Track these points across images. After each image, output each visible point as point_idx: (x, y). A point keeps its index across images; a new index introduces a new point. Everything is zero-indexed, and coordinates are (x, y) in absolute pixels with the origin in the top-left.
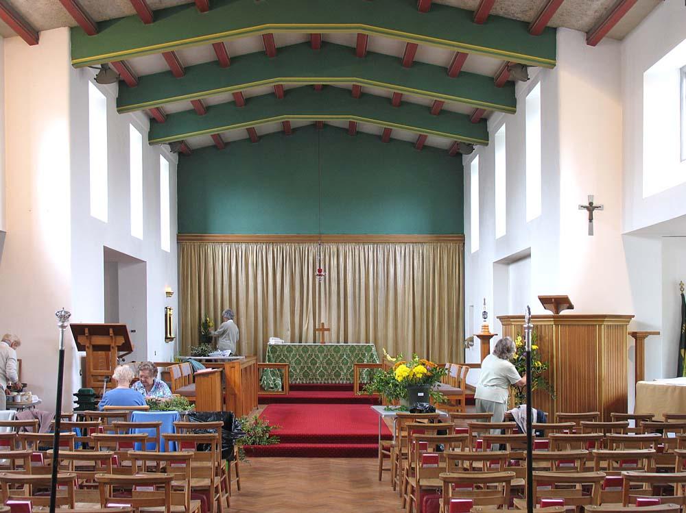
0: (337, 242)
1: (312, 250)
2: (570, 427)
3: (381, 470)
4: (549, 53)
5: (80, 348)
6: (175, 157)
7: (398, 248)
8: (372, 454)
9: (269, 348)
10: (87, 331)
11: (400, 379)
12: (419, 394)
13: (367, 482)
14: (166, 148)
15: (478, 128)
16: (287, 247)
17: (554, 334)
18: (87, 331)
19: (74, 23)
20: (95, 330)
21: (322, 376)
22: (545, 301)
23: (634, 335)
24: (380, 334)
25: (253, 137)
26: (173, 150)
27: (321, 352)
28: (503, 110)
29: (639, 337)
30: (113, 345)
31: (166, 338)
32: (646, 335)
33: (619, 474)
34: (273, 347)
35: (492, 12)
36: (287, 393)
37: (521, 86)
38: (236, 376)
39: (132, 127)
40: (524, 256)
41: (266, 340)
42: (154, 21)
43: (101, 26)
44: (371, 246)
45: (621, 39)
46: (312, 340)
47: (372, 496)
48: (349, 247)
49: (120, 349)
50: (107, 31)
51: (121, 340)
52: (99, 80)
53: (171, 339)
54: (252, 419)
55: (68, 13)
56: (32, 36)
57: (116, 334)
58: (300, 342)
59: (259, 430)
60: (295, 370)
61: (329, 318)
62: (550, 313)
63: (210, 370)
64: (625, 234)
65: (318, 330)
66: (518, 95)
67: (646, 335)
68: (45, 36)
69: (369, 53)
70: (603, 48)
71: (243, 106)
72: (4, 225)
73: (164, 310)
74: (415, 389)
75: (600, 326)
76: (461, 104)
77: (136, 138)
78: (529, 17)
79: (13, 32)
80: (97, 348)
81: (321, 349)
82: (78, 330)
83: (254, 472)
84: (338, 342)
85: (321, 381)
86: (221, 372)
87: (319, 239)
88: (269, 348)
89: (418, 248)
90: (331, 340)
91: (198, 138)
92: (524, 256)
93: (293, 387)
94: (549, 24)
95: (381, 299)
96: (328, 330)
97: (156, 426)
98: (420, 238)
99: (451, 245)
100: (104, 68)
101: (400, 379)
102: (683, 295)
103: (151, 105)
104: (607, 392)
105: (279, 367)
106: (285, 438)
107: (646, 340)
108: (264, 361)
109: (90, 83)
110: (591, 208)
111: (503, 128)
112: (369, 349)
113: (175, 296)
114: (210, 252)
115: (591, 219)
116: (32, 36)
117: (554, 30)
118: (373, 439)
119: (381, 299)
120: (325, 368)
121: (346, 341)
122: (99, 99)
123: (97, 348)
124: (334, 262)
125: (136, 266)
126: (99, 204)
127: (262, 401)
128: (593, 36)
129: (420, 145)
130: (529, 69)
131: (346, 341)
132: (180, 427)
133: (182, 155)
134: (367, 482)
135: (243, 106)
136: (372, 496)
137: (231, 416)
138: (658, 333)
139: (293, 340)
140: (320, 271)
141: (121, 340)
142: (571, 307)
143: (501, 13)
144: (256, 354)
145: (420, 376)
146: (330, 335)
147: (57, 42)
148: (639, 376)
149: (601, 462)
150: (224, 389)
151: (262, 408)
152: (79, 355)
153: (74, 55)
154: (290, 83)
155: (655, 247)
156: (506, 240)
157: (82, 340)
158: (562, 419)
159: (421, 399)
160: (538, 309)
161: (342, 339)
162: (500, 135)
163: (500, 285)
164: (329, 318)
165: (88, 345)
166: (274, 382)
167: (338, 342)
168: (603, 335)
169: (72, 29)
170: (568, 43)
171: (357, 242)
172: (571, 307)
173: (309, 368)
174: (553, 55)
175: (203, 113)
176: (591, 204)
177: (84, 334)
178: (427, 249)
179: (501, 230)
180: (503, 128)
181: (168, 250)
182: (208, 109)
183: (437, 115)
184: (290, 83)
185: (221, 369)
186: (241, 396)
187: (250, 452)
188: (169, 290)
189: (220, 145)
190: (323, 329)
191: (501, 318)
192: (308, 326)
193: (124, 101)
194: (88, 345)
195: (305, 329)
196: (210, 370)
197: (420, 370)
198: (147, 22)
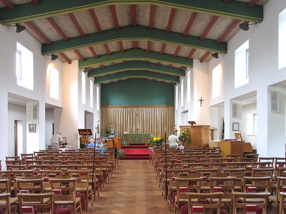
0: (141, 107)
1: (135, 109)
2: (201, 154)
3: (150, 161)
4: (191, 64)
5: (80, 135)
6: (100, 87)
7: (157, 109)
8: (148, 159)
9: (124, 135)
10: (82, 131)
11: (154, 141)
13: (146, 164)
14: (98, 85)
15: (178, 80)
17: (192, 130)
18: (87, 131)
19: (80, 59)
20: (83, 130)
21: (137, 141)
22: (189, 122)
23: (211, 130)
24: (153, 130)
26: (100, 85)
27: (137, 135)
28: (183, 76)
29: (212, 131)
30: (88, 134)
32: (214, 130)
34: (125, 134)
35: (178, 55)
36: (128, 146)
37: (186, 72)
38: (116, 141)
39: (91, 80)
40: (187, 111)
41: (123, 132)
42: (98, 58)
43: (86, 59)
45: (208, 61)
46: (129, 132)
47: (148, 166)
49: (89, 135)
50: (87, 60)
51: (90, 133)
52: (85, 71)
53: (99, 133)
54: (121, 151)
55: (77, 56)
56: (70, 62)
57: (88, 131)
58: (132, 133)
59: (122, 153)
60: (131, 140)
61: (139, 127)
62: (191, 125)
63: (110, 139)
64: (210, 106)
65: (97, 139)
66: (180, 79)
67: (214, 130)
69: (154, 28)
70: (204, 63)
71: (114, 66)
72: (63, 106)
73: (97, 125)
74: (158, 143)
76: (177, 65)
77: (92, 83)
78: (186, 56)
79: (65, 61)
80: (84, 135)
81: (137, 135)
82: (80, 130)
83: (121, 163)
85: (137, 143)
86: (113, 140)
87: (137, 107)
88: (124, 135)
89: (163, 109)
90: (140, 132)
91: (106, 82)
92: (187, 111)
93: (130, 144)
94: (191, 58)
95: (153, 122)
96: (139, 130)
97: (101, 151)
98: (163, 106)
99: (171, 108)
100: (86, 69)
101: (154, 141)
102: (223, 121)
103: (96, 76)
104: (204, 143)
105: (126, 139)
106: (128, 155)
107: (214, 131)
108: (123, 138)
109: (82, 72)
110: (201, 100)
111: (183, 80)
112: (150, 134)
113: (100, 122)
115: (201, 103)
116: (70, 62)
117: (193, 59)
118: (149, 155)
119: (153, 122)
120: (138, 139)
121: (144, 133)
122: (84, 75)
123: (84, 135)
124: (141, 112)
126: (84, 101)
127: (122, 148)
128: (202, 60)
129: (163, 83)
130: (187, 68)
131: (144, 133)
132: (105, 151)
134: (146, 164)
136: (148, 166)
137: (116, 149)
138: (217, 130)
139: (130, 133)
140: (137, 115)
141: (90, 133)
142: (195, 124)
143: (180, 55)
144: (120, 136)
145: (159, 140)
146: (140, 131)
147: (75, 63)
148: (212, 139)
149: (285, 199)
150: (113, 145)
151: (122, 150)
152: (79, 136)
153: (79, 66)
154: (128, 60)
155: (216, 109)
156: (183, 107)
157: (80, 133)
158: (190, 148)
159: (159, 145)
160: (189, 125)
161: (143, 132)
162: (182, 81)
163: (183, 117)
164: (139, 127)
165: (82, 134)
166: (125, 143)
168: (203, 130)
169: (79, 60)
170: (196, 62)
172: (195, 124)
173: (134, 139)
174: (192, 65)
176: (201, 99)
177: (87, 131)
178: (165, 109)
179: (182, 105)
180: (183, 80)
182: (105, 67)
183: (167, 76)
184: (128, 60)
185: (113, 139)
186: (118, 146)
187: (121, 158)
189: (112, 83)
190: (138, 130)
191: (180, 126)
192: (134, 129)
193: (89, 75)
194: (82, 134)
195: (133, 129)
196: (110, 139)
197: (159, 138)
198: (96, 58)
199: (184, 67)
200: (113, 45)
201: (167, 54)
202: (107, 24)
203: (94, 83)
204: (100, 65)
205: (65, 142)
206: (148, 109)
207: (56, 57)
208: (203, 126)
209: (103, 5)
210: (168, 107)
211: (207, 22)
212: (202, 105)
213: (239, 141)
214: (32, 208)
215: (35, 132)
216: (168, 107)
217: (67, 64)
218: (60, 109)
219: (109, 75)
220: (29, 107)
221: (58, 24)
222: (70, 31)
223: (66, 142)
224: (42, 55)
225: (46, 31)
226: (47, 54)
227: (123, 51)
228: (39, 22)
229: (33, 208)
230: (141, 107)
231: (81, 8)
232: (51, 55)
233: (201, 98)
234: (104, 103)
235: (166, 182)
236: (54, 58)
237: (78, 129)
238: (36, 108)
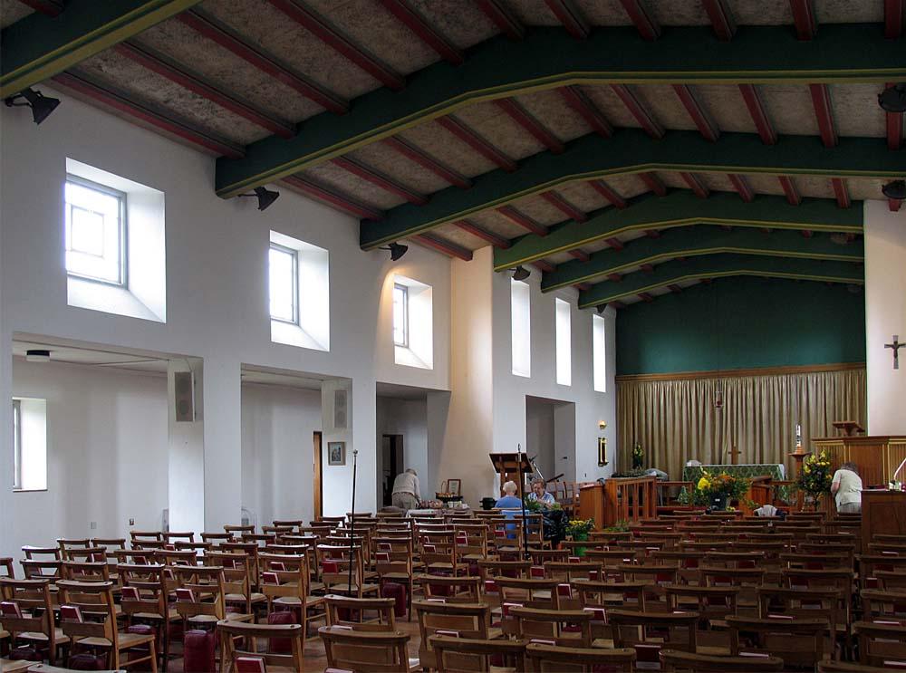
0: (753, 375)
9: (684, 470)
10: (500, 458)
12: (717, 500)
16: (708, 382)
18: (500, 458)
25: (676, 292)
31: (599, 463)
33: (662, 518)
43: (513, 242)
44: (784, 377)
46: (710, 461)
48: (764, 379)
56: (467, 255)
68: (475, 254)
71: (620, 251)
72: (449, 387)
75: (886, 445)
84: (754, 463)
87: (735, 374)
88: (684, 470)
91: (630, 296)
110: (896, 346)
114: (642, 390)
115: (896, 356)
117: (861, 203)
121: (761, 462)
124: (750, 393)
125: (569, 405)
126: (521, 361)
131: (761, 462)
133: (618, 310)
135: (654, 272)
147: (484, 255)
153: (495, 265)
161: (758, 460)
167: (754, 463)
171: (772, 374)
175: (621, 281)
176: (896, 343)
181: (604, 390)
188: (603, 424)
189: (648, 300)
192: (727, 448)
199: (834, 233)
200: (578, 192)
201: (766, 196)
202: (519, 143)
203: (579, 304)
204: (607, 241)
205: (456, 492)
206: (774, 380)
207: (404, 249)
208: (889, 437)
209: (370, 140)
210: (852, 369)
211: (806, 91)
212: (899, 364)
213: (893, 492)
214: (258, 662)
215: (344, 464)
216: (848, 369)
217: (459, 263)
218: (444, 396)
219: (656, 267)
220: (328, 392)
221: (376, 165)
222: (418, 177)
223: (459, 492)
224: (362, 248)
225: (352, 187)
226: (380, 245)
227: (621, 207)
228: (324, 170)
229: (262, 665)
230: (747, 375)
231: (366, 138)
232: (389, 245)
233: (896, 337)
234: (626, 366)
235: (350, 581)
236: (398, 252)
237: (491, 455)
238: (342, 399)
